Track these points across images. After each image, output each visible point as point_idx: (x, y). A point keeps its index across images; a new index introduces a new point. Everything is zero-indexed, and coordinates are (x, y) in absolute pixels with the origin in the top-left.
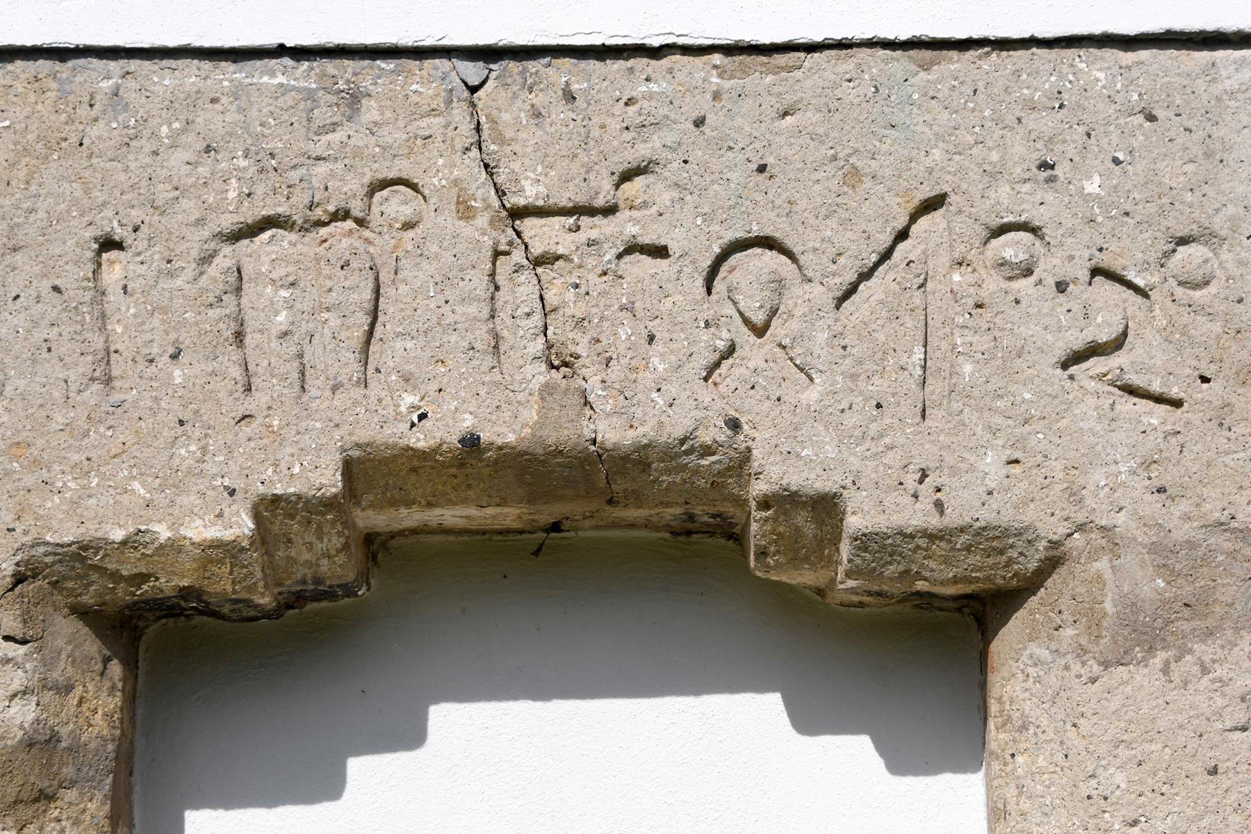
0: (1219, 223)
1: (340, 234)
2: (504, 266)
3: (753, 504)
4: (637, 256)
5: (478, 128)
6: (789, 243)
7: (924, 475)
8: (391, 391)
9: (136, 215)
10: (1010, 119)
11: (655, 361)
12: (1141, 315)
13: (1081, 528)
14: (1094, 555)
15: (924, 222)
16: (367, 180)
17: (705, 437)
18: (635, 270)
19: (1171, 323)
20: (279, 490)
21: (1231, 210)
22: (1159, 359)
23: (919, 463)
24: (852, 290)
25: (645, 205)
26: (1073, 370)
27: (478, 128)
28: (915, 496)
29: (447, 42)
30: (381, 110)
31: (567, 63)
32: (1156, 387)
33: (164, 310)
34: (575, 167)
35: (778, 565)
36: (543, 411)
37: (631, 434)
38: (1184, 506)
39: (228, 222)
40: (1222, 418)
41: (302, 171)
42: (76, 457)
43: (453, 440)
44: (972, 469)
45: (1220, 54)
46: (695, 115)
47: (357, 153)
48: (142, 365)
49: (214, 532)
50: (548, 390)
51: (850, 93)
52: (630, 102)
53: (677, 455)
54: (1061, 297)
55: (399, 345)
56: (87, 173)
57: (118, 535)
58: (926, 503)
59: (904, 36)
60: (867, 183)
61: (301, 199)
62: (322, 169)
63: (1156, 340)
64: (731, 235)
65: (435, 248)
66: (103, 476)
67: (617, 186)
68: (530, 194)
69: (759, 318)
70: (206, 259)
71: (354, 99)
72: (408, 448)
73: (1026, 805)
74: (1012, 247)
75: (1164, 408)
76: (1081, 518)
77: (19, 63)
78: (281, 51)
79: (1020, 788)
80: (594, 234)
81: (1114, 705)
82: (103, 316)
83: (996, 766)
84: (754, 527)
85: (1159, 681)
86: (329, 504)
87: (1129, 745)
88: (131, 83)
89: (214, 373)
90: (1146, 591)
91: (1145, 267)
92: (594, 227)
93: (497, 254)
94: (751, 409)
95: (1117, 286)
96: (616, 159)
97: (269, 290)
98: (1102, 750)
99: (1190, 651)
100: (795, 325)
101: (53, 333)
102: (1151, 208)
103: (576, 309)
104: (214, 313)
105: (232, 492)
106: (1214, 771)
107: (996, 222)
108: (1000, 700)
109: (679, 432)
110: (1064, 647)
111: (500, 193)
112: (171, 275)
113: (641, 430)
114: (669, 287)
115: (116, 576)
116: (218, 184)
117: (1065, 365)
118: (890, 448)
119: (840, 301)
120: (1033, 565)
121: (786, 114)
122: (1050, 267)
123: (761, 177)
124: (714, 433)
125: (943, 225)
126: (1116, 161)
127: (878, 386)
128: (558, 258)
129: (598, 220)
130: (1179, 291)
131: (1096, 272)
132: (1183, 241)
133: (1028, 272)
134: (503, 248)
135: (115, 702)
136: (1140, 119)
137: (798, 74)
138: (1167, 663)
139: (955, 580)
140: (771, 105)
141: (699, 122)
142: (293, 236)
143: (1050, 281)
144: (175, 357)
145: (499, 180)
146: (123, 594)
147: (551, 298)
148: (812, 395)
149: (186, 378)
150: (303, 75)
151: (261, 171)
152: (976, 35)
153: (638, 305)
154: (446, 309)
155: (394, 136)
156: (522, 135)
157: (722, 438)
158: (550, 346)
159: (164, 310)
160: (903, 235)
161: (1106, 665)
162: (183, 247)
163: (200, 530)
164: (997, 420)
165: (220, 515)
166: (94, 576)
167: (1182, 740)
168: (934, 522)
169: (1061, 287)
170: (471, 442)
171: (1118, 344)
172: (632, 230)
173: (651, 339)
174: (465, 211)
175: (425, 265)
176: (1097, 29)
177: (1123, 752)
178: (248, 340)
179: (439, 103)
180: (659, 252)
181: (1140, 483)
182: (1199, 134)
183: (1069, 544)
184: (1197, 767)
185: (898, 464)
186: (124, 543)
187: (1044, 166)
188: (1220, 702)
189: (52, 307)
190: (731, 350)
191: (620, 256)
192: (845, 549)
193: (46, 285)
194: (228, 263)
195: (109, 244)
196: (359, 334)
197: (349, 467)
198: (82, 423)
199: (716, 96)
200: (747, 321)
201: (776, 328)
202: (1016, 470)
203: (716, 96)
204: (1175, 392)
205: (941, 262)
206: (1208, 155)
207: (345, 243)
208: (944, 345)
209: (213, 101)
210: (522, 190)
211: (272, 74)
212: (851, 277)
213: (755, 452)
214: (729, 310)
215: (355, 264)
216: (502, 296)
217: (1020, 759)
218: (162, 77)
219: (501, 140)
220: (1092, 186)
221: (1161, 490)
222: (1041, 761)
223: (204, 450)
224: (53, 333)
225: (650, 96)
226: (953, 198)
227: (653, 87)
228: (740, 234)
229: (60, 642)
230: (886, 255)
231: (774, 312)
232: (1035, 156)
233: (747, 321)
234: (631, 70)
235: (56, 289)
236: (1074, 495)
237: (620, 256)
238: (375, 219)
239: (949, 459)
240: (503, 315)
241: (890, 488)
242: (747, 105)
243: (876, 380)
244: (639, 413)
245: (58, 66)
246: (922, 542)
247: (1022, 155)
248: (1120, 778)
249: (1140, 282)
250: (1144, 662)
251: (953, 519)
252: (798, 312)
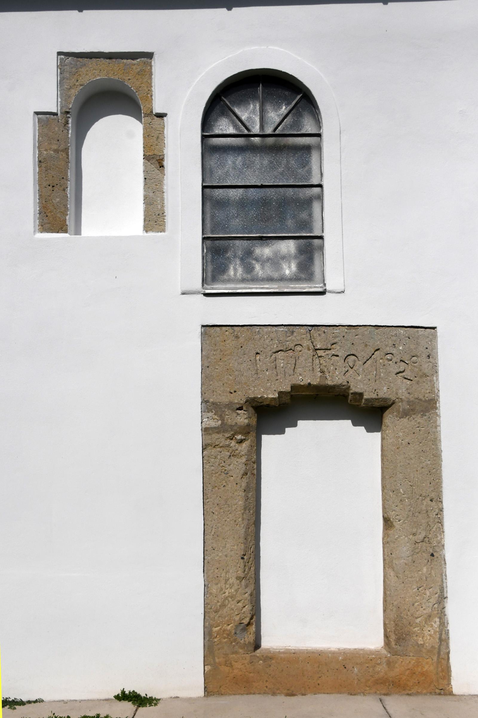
0: (418, 354)
1: (290, 353)
2: (314, 358)
3: (350, 394)
4: (334, 356)
5: (311, 337)
6: (356, 355)
7: (375, 390)
8: (298, 376)
9: (262, 349)
10: (389, 337)
11: (337, 372)
12: (407, 367)
13: (397, 398)
14: (399, 402)
15: (376, 352)
16: (295, 344)
17: (344, 384)
18: (333, 358)
19: (411, 369)
20: (282, 390)
21: (420, 352)
22: (409, 374)
23: (375, 388)
24: (366, 362)
25: (335, 349)
26: (397, 375)
27: (311, 337)
28: (374, 393)
29: (307, 324)
30: (297, 334)
31: (324, 327)
32: (409, 378)
33: (266, 364)
34: (325, 343)
35: (353, 402)
36: (320, 379)
37: (333, 383)
38: (412, 396)
39: (274, 350)
40: (418, 383)
41: (285, 343)
42: (253, 385)
43: (307, 383)
44: (382, 390)
45: (419, 329)
46: (343, 335)
47: (293, 340)
48: (262, 371)
49: (273, 396)
50: (321, 376)
51: (366, 333)
52: (333, 333)
53: (339, 386)
54: (396, 364)
55: (299, 369)
56: (255, 343)
57: (259, 396)
58: (375, 395)
59: (374, 325)
60: (368, 346)
61: (285, 347)
62: (288, 343)
63: (409, 371)
64: (348, 354)
65: (304, 355)
66: (257, 388)
67: (331, 346)
68: (318, 347)
69: (352, 366)
70: (271, 356)
71: (293, 332)
72: (300, 385)
73: (387, 437)
74: (389, 357)
75: (410, 381)
76: (397, 397)
77: (245, 327)
78: (282, 325)
79: (387, 435)
80: (328, 353)
81: (401, 424)
82: (256, 364)
83: (383, 432)
84: (350, 397)
85: (407, 420)
86: (289, 392)
87: (403, 429)
88: (261, 330)
89: (272, 373)
90: (406, 408)
91: (408, 360)
92: (328, 352)
93: (313, 356)
94: (351, 380)
95: (404, 363)
96: (331, 342)
97: (280, 361)
98: (399, 430)
99: (412, 416)
100: (357, 367)
101: (250, 367)
102: (409, 352)
103: (324, 364)
104: (272, 364)
105: (275, 391)
106: (414, 433)
107: (387, 353)
108: (384, 422)
109: (340, 383)
110: (394, 415)
111: (314, 347)
112: (266, 358)
113: (334, 383)
114: (339, 361)
115: (258, 402)
116: (273, 345)
117: (396, 374)
118: (371, 386)
119: (364, 364)
120: (390, 403)
121: (356, 336)
122: (394, 360)
123: (353, 345)
124: (345, 383)
125: (379, 353)
126: (404, 344)
127: (369, 377)
128: (322, 356)
129: (328, 351)
130: (413, 364)
131: (401, 361)
132: (413, 357)
133: (391, 360)
134: (314, 355)
135: (256, 420)
136: (407, 338)
137: (358, 330)
138: (408, 418)
139: (379, 405)
140: (354, 334)
141: (344, 337)
142: (283, 353)
143: (394, 362)
144: (267, 370)
145: (314, 345)
146: (259, 404)
147: (321, 362)
148: (359, 378)
149: (269, 374)
150: (285, 329)
151: (279, 343)
152: (384, 325)
153: (334, 364)
154: (306, 364)
155: (299, 338)
156: (317, 338)
157: (346, 384)
158: (321, 369)
159: (266, 364)
160: (373, 354)
161: (400, 418)
162: (268, 354)
163: (271, 396)
164: (386, 382)
165: (273, 394)
166: (255, 402)
167: (410, 429)
168: (377, 397)
169: (396, 363)
170: (309, 384)
171: (403, 372)
172: (333, 352)
173: (336, 369)
174: (309, 349)
175: (303, 357)
176: (402, 325)
177: (402, 430)
178: (277, 368)
179: (305, 333)
180: (337, 356)
181: (406, 392)
182: (416, 341)
183: (396, 401)
184: (412, 433)
185: (372, 389)
186: (260, 397)
187: (394, 345)
188: (415, 423)
189: (250, 363)
190: (348, 371)
191: (331, 356)
192: (363, 401)
193: (249, 360)
194: (274, 357)
195: (257, 353)
196: (293, 368)
197: (292, 387)
198: (254, 380)
199: (346, 333)
200: (350, 367)
201: (354, 368)
202: (389, 390)
203: (346, 333)
204: (411, 379)
205: (379, 358)
206: (417, 344)
207: (291, 354)
208: (379, 371)
209: (273, 332)
210: (317, 346)
211: (281, 329)
212: (366, 360)
213: (351, 386)
214: (347, 365)
215: (293, 357)
216: (314, 362)
217: (387, 431)
218: (265, 329)
219: (314, 339)
220: (401, 348)
221: (409, 393)
222: (390, 432)
223: (271, 384)
224: (250, 367)
225: (336, 332)
226: (381, 349)
227: (337, 331)
228: (349, 354)
229: (250, 411)
230: (371, 357)
231: (354, 365)
232: (393, 343)
233: (350, 367)
234: (334, 328)
235: (250, 360)
236: (397, 394)
237: (331, 356)
238: (296, 350)
239: (379, 388)
240: (314, 365)
241: (371, 392)
242: (351, 334)
243: (369, 376)
244: (334, 380)
245: (251, 327)
246: (375, 400)
247: (391, 343)
248: (401, 434)
249: (407, 362)
250: (405, 418)
251: (379, 397)
252: (358, 365)
